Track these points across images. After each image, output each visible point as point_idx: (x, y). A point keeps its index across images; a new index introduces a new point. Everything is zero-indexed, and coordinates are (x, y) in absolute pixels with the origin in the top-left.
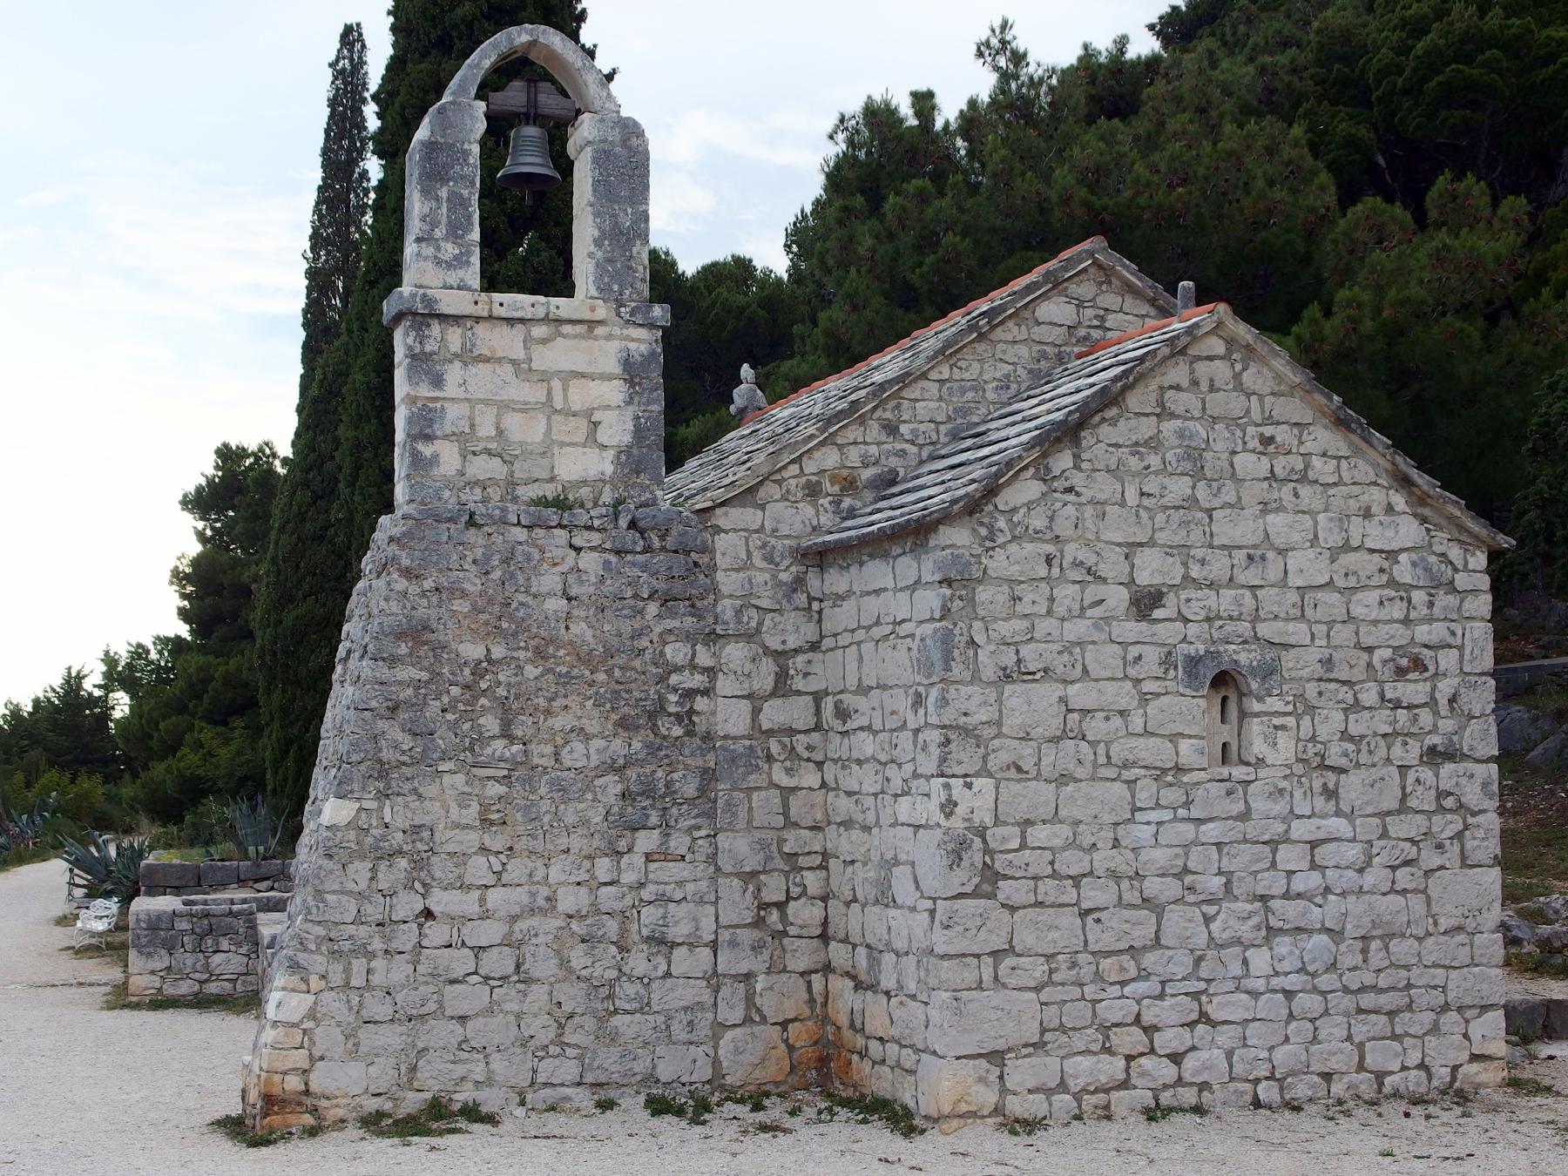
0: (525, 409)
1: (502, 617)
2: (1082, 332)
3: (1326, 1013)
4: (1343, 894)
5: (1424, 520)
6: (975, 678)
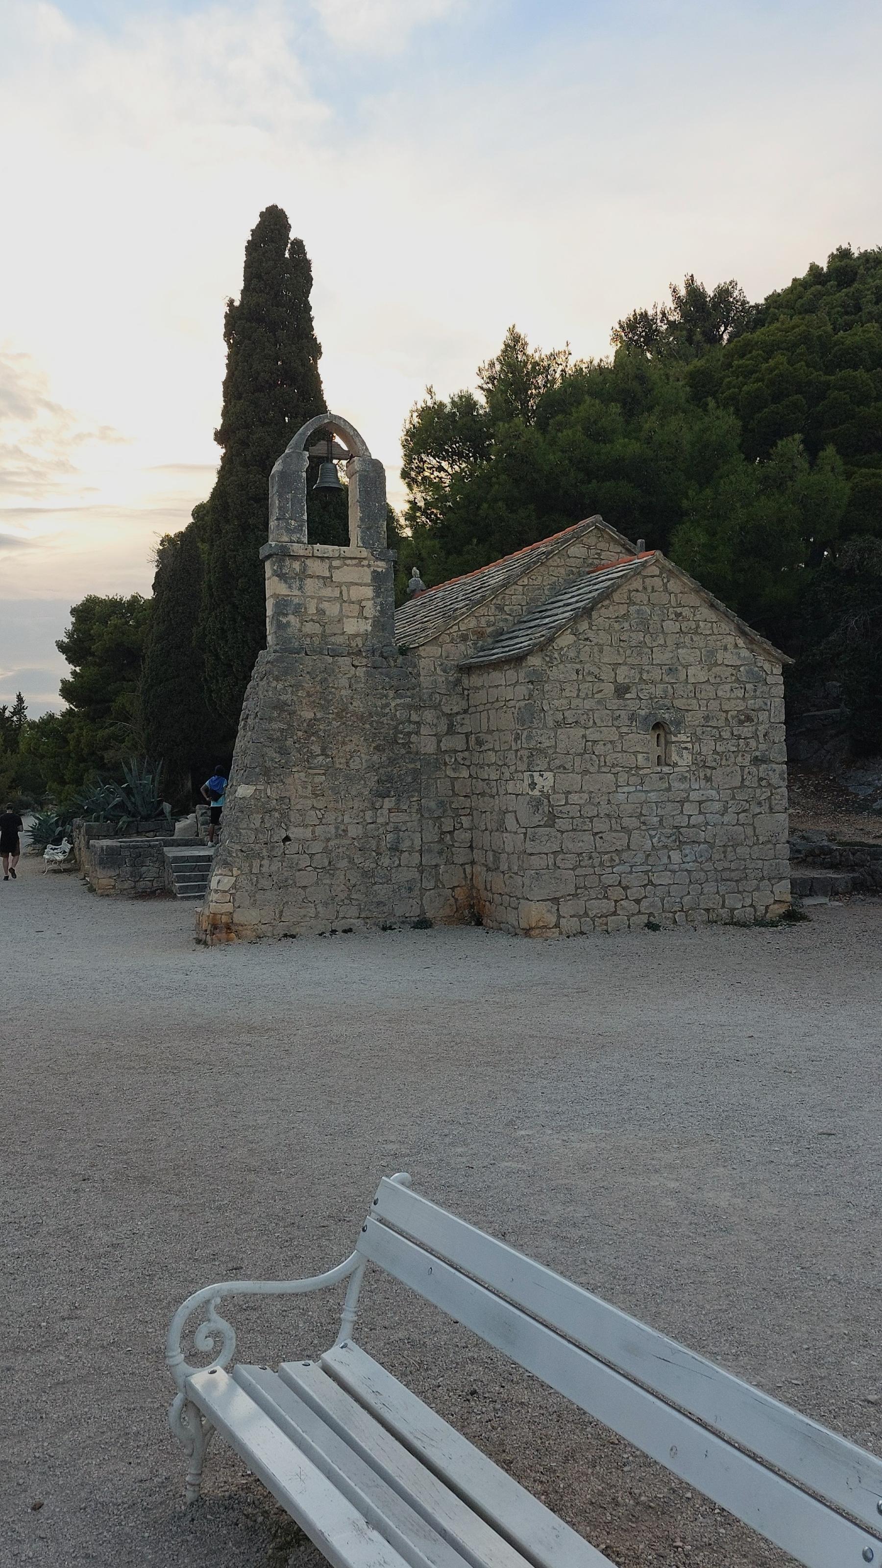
0: (330, 600)
2: (590, 561)
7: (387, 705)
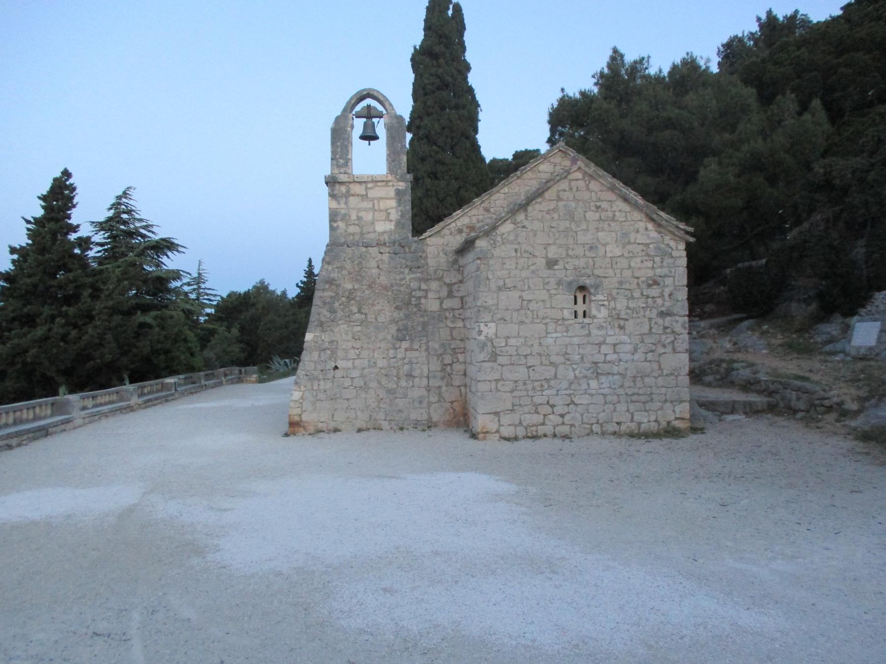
0: (366, 210)
1: (358, 275)
3: (619, 402)
4: (626, 362)
5: (660, 233)
7: (404, 279)
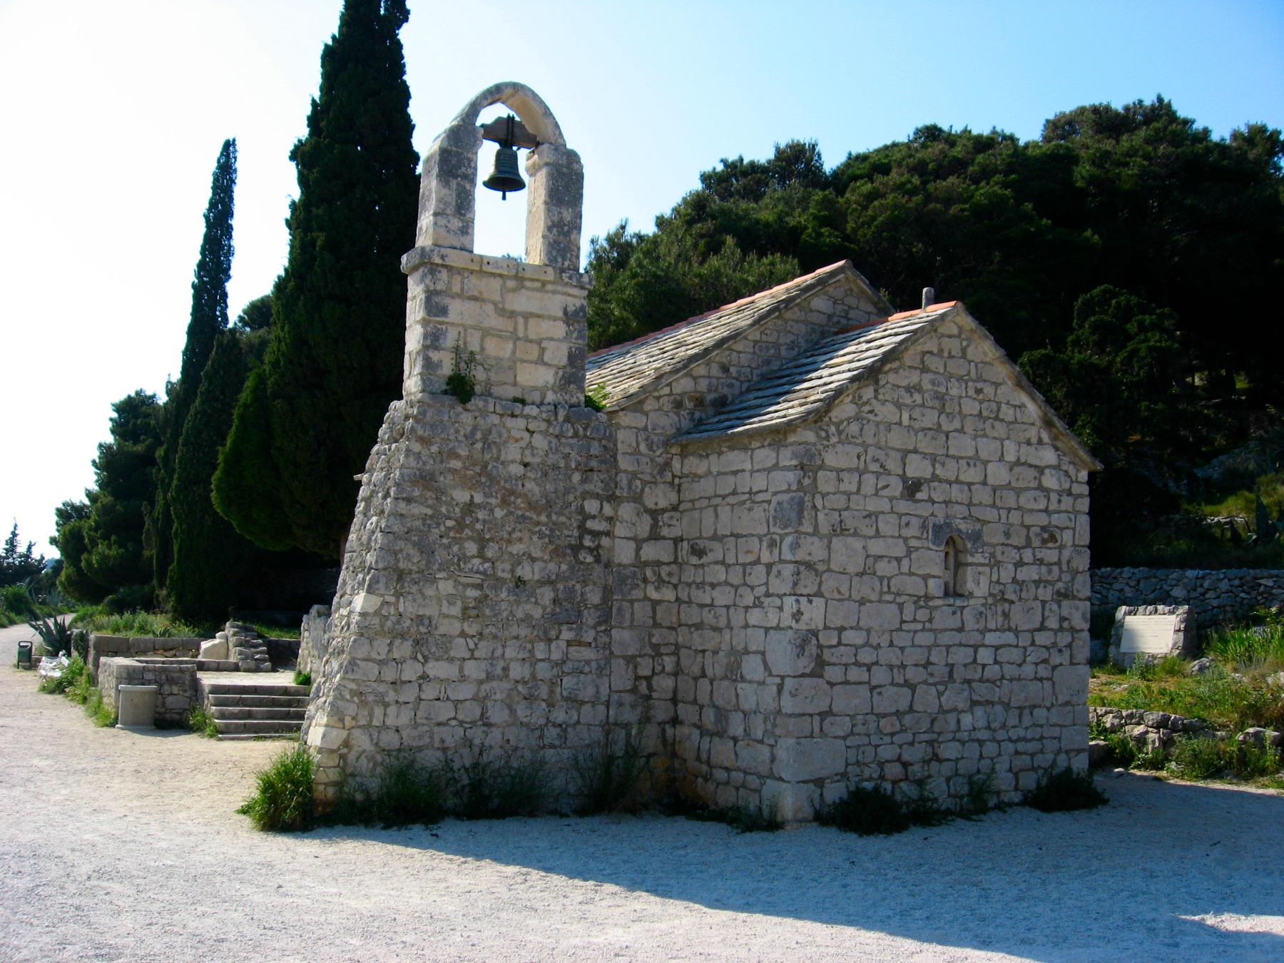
2: (835, 319)
5: (1057, 449)
6: (816, 532)
